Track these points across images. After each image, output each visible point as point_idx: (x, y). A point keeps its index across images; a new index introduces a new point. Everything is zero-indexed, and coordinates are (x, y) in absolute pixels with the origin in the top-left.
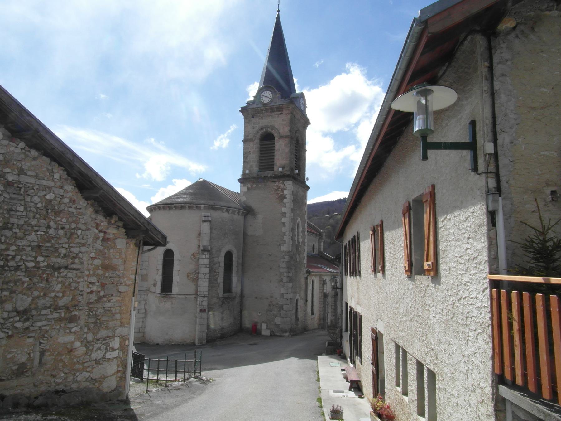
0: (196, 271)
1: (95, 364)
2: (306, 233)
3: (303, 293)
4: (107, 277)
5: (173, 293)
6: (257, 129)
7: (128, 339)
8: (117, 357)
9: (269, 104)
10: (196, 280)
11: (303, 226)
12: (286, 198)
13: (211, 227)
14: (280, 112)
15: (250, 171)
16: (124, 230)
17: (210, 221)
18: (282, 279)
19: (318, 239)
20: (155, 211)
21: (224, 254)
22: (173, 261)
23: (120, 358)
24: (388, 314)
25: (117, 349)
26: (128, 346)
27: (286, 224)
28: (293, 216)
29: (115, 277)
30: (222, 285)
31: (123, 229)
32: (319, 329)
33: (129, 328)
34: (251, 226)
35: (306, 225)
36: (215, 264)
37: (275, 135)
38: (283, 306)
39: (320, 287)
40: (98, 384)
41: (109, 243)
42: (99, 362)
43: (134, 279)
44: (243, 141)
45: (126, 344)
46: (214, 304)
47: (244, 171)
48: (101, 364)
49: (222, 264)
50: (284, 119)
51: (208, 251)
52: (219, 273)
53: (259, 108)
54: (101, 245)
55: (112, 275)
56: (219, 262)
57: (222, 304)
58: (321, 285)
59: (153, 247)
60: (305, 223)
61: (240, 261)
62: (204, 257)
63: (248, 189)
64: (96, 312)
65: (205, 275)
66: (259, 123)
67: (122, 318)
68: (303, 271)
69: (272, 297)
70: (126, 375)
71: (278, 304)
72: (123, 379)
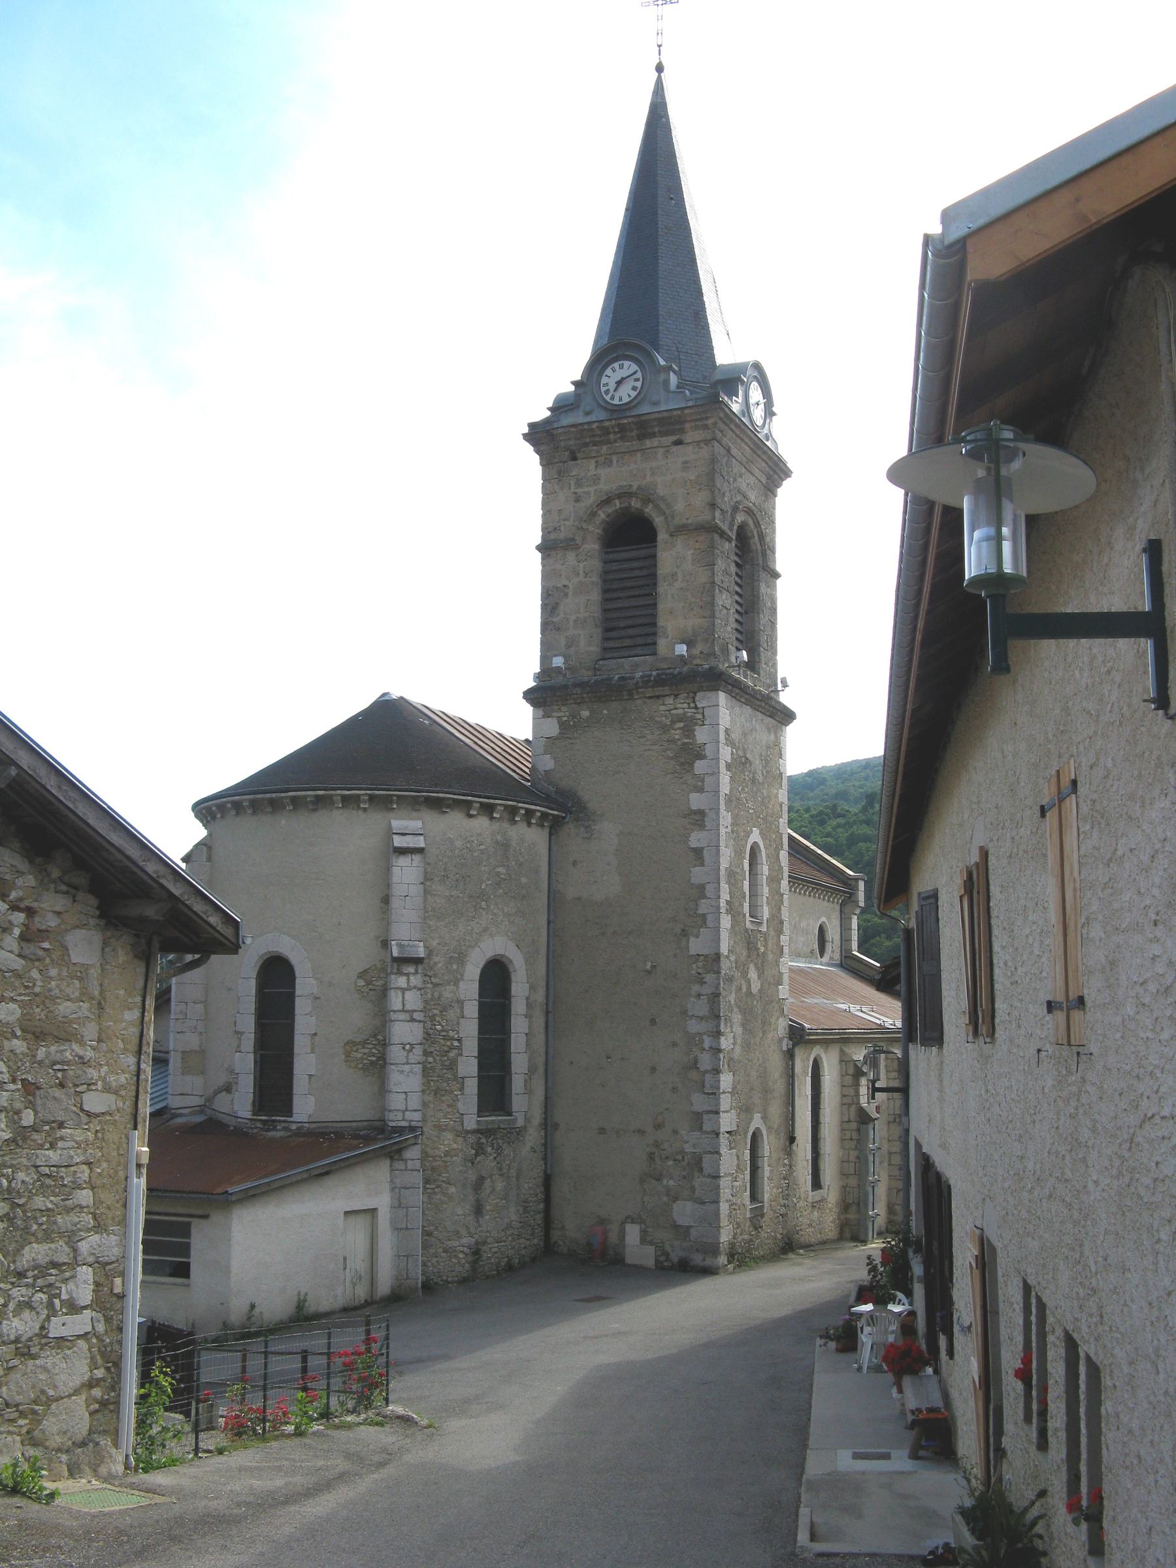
0: (375, 1036)
1: (16, 1355)
2: (785, 884)
3: (776, 1109)
4: (40, 1063)
5: (296, 1118)
6: (590, 501)
7: (122, 1274)
8: (87, 1333)
9: (630, 409)
10: (378, 1066)
11: (774, 859)
12: (704, 757)
13: (426, 873)
14: (674, 438)
15: (567, 658)
16: (94, 902)
17: (420, 851)
18: (696, 1061)
19: (838, 907)
20: (222, 817)
21: (478, 971)
22: (293, 1002)
23: (97, 1337)
24: (1004, 1180)
25: (85, 1308)
26: (122, 1297)
27: (705, 852)
28: (732, 824)
29: (68, 1063)
30: (472, 1086)
31: (90, 896)
32: (841, 1238)
33: (125, 1235)
34: (575, 863)
35: (784, 855)
36: (444, 1010)
37: (658, 521)
38: (701, 1159)
39: (843, 1086)
40: (27, 1421)
41: (46, 945)
42: (29, 1347)
43: (133, 1068)
44: (539, 548)
45: (116, 1291)
46: (447, 1154)
47: (545, 659)
48: (34, 1357)
49: (472, 1010)
50: (687, 462)
51: (417, 961)
52: (459, 1040)
53: (594, 426)
54: (20, 956)
55: (58, 1057)
56: (461, 1003)
57: (477, 1155)
58: (849, 1080)
59: (197, 956)
60: (779, 847)
61: (540, 996)
62: (405, 985)
63: (563, 726)
64: (10, 1182)
65: (410, 1051)
66: (596, 479)
67: (98, 1202)
68: (776, 1029)
69: (658, 1126)
70: (119, 1395)
71: (682, 1152)
72: (111, 1407)
